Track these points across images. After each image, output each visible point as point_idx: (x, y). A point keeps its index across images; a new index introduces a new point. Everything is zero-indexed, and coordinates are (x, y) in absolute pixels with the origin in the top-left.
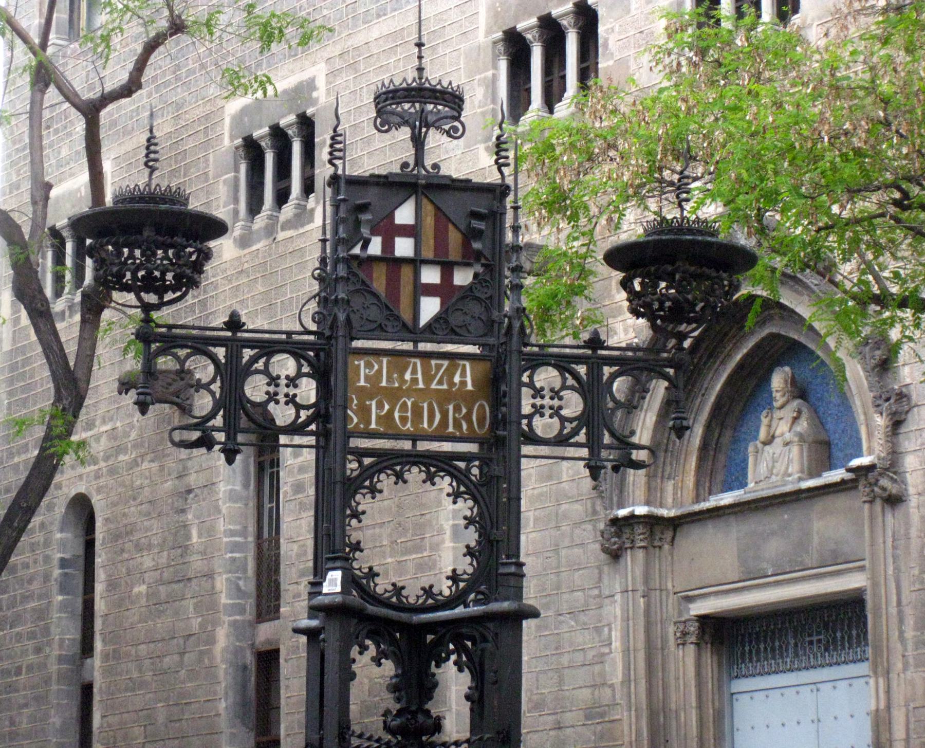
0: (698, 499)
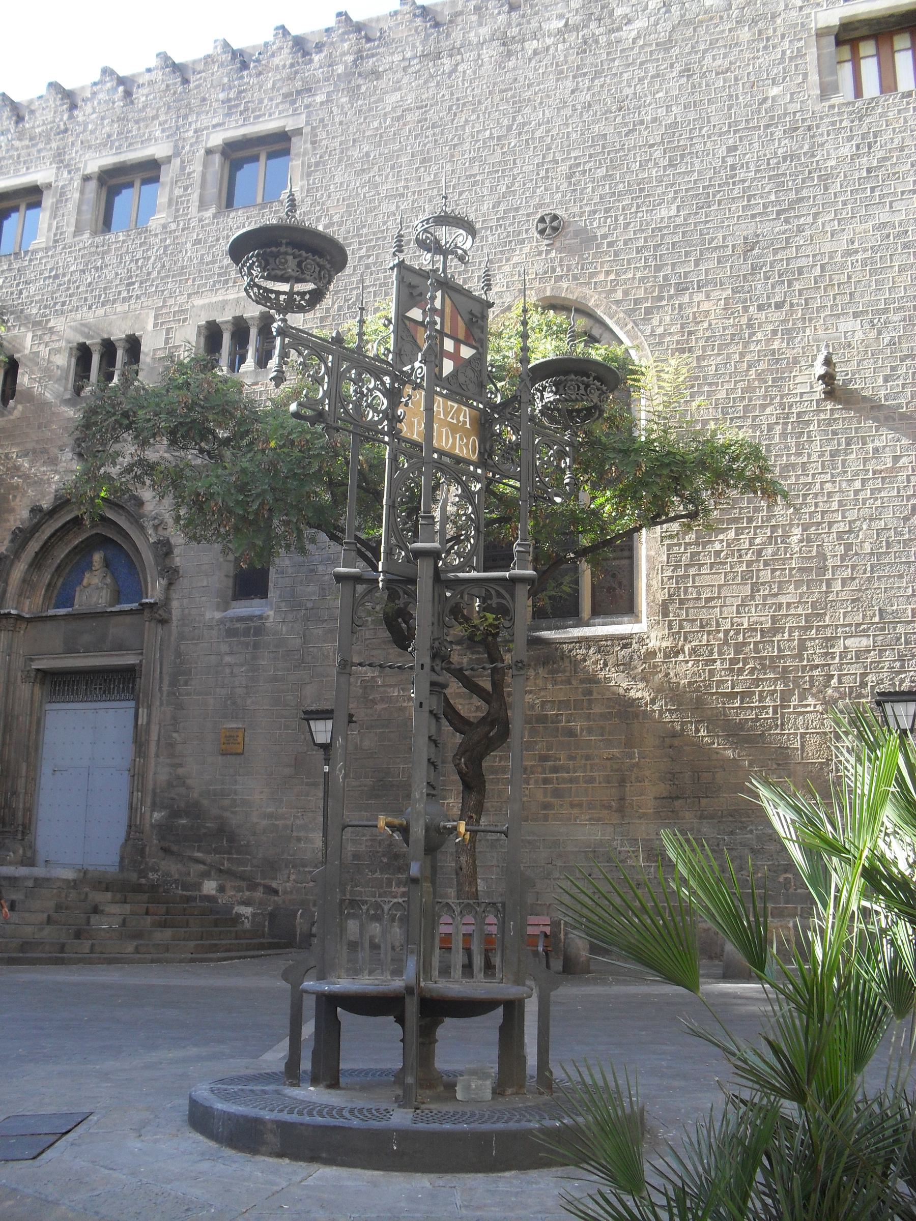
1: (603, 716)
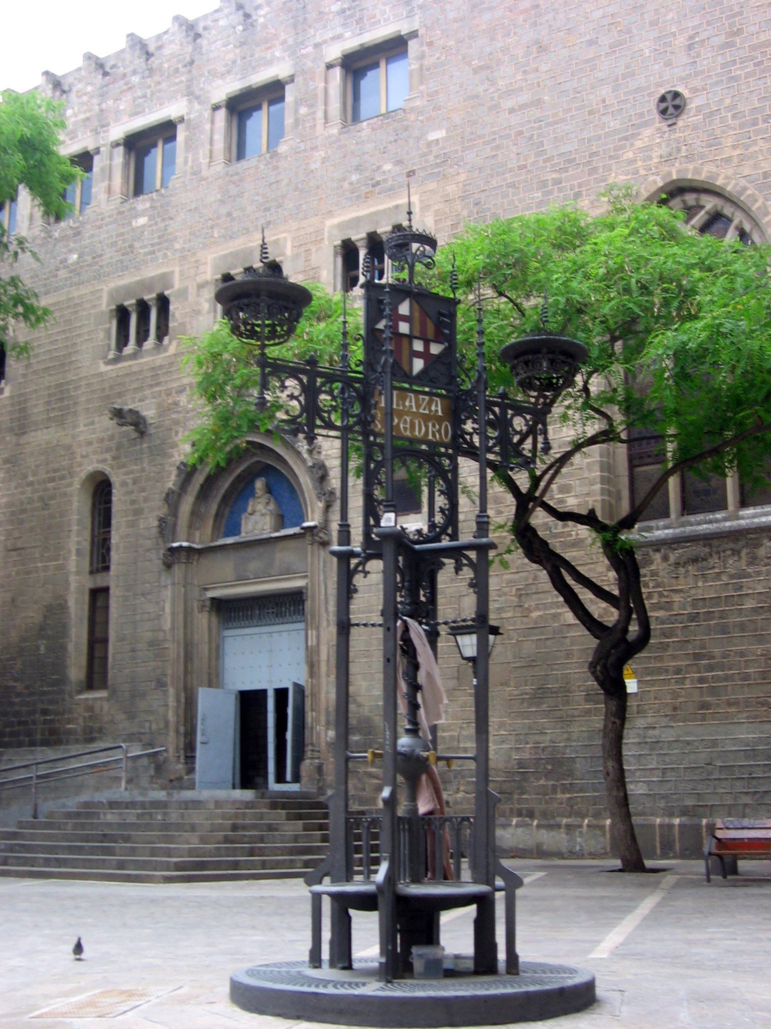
0: (212, 540)
1: (755, 610)
